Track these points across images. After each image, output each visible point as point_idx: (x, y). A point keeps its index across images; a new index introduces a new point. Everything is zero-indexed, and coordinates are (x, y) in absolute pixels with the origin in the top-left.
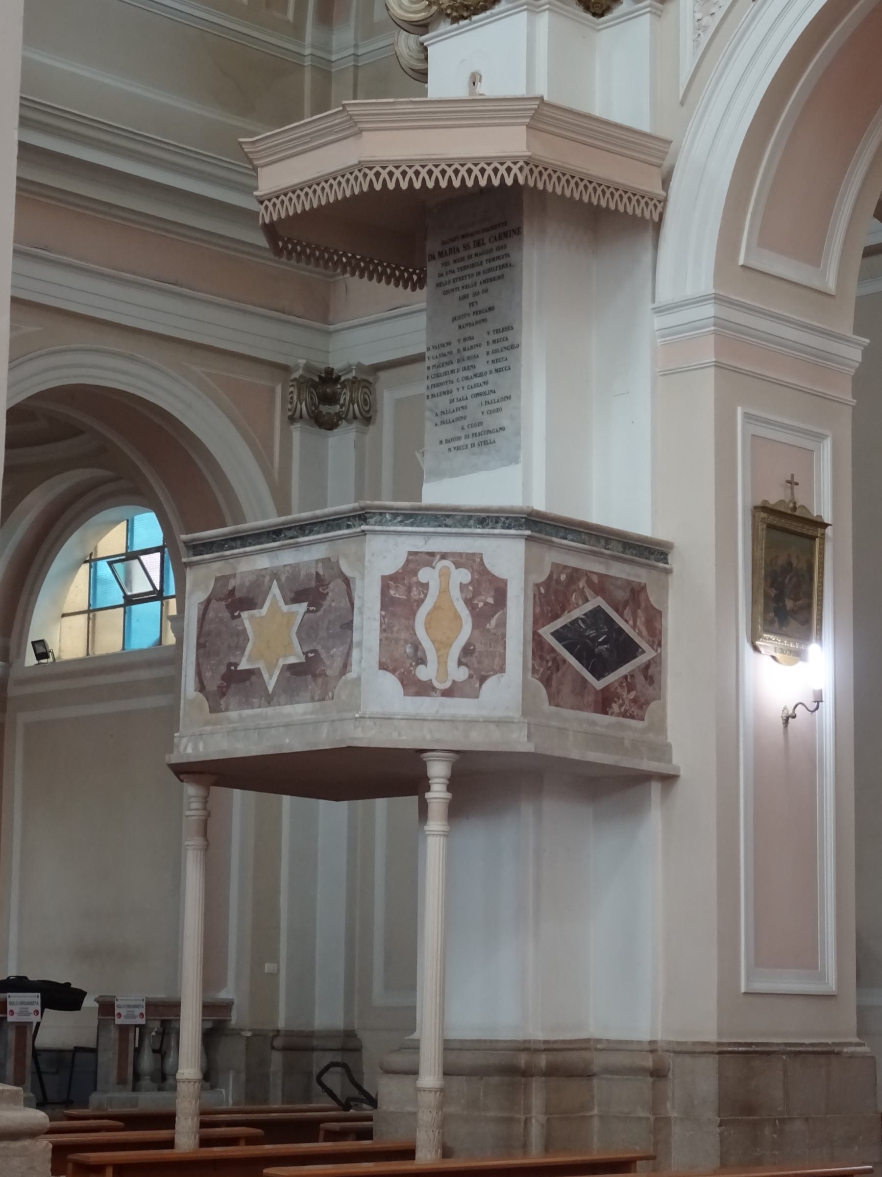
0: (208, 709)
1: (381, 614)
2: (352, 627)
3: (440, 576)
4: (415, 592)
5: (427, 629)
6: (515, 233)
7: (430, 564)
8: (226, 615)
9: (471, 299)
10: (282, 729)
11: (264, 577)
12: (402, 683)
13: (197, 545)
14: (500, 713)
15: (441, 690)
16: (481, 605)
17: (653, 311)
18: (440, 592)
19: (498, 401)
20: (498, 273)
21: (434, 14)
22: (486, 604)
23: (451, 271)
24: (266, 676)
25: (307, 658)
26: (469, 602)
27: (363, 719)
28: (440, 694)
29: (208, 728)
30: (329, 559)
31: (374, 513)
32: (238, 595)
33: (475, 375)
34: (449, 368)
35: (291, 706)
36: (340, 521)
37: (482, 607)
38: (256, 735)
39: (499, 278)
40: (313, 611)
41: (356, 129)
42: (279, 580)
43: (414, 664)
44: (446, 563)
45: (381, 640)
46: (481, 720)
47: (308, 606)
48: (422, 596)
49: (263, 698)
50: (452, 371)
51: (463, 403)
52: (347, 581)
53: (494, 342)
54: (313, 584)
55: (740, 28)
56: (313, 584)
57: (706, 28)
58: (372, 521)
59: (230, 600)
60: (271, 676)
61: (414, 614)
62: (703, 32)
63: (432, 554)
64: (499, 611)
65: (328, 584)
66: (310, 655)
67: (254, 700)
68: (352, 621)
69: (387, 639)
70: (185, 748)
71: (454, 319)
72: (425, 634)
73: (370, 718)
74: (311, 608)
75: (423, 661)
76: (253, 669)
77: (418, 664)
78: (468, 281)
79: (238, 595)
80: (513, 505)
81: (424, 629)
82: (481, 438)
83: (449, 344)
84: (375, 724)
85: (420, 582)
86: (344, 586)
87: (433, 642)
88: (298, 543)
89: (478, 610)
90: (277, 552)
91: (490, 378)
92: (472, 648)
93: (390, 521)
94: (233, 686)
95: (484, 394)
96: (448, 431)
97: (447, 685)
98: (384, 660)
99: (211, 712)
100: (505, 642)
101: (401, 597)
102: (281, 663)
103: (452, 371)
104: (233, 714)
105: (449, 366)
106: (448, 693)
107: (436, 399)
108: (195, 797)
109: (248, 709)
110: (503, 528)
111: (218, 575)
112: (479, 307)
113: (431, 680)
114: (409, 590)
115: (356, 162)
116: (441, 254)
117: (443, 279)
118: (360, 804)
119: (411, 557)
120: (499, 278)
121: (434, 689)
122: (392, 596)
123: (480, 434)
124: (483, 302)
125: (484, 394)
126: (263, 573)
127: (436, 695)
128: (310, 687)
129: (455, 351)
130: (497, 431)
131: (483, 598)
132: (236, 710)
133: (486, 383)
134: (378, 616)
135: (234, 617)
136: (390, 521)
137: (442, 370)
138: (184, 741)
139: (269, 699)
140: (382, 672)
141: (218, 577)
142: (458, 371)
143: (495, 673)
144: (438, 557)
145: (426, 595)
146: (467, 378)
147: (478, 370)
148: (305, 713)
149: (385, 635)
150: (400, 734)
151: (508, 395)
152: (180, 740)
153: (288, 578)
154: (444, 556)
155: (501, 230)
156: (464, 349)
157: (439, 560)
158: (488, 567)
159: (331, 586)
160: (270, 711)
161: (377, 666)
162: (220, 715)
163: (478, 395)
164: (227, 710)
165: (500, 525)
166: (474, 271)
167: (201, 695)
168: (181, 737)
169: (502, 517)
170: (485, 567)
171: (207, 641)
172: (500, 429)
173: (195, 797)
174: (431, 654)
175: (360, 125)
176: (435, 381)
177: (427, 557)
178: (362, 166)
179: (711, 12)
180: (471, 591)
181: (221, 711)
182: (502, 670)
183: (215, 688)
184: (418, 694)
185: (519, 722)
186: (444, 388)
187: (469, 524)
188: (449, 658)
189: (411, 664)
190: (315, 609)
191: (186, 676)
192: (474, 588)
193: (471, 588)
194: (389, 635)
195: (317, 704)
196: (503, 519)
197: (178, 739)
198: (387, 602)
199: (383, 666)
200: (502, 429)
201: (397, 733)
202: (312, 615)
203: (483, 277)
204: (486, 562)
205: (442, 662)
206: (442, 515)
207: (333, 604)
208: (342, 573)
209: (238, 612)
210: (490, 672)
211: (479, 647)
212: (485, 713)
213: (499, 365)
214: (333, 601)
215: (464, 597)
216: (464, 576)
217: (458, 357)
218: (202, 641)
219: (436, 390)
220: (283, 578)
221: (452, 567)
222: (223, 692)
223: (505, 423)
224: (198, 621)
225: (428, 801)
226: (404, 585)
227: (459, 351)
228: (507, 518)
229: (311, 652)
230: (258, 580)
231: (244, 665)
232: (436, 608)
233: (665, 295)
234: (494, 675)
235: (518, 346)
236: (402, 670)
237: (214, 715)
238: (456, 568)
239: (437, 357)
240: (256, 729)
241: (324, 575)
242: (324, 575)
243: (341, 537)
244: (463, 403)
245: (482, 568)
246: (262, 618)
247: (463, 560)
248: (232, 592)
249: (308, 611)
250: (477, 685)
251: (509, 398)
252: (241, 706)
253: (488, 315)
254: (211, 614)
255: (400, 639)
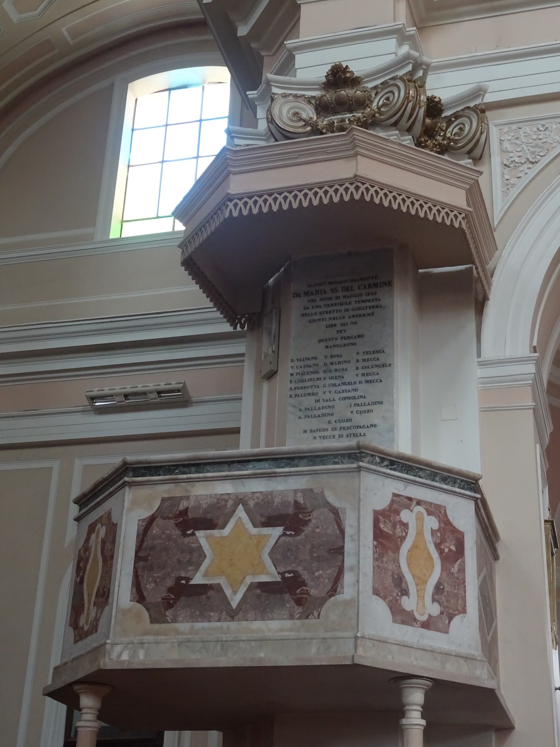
0: (149, 619)
1: (373, 544)
2: (344, 552)
3: (417, 519)
4: (398, 530)
5: (409, 565)
6: (386, 285)
7: (408, 507)
8: (176, 532)
9: (339, 328)
10: (253, 644)
11: (227, 501)
12: (391, 609)
13: (138, 468)
14: (464, 650)
15: (421, 622)
16: (446, 550)
17: (478, 364)
18: (417, 533)
19: (369, 404)
20: (368, 311)
21: (308, 131)
22: (450, 550)
23: (317, 307)
24: (228, 592)
25: (283, 578)
26: (438, 546)
27: (364, 639)
28: (420, 625)
29: (150, 638)
30: (312, 490)
31: (368, 454)
32: (190, 515)
33: (344, 384)
34: (315, 376)
35: (263, 622)
36: (325, 458)
37: (447, 552)
38: (219, 647)
39: (369, 315)
40: (290, 535)
41: (353, 152)
42: (245, 505)
43: (399, 594)
44: (420, 509)
45: (374, 568)
46: (454, 654)
47: (284, 530)
48: (404, 534)
49: (224, 613)
50: (318, 379)
51: (331, 404)
52: (335, 512)
53: (364, 360)
54: (291, 510)
55: (552, 186)
56: (291, 510)
57: (513, 185)
58: (366, 460)
59: (182, 519)
60: (235, 593)
61: (397, 549)
62: (511, 187)
63: (410, 499)
64: (460, 559)
65: (311, 512)
66: (287, 575)
67: (212, 614)
68: (343, 547)
69: (379, 567)
70: (120, 655)
71: (320, 341)
72: (407, 568)
73: (370, 639)
74: (288, 533)
75: (405, 592)
76: (211, 584)
77: (403, 595)
78: (335, 315)
79: (190, 515)
80: (469, 470)
81: (406, 565)
82: (350, 431)
83: (315, 358)
84: (373, 645)
85: (402, 521)
86: (332, 515)
87: (414, 576)
88: (276, 473)
89: (444, 554)
90: (244, 480)
91: (361, 387)
92: (442, 587)
93: (379, 463)
94: (183, 598)
95: (354, 398)
96: (307, 424)
97: (425, 618)
98: (376, 586)
99: (151, 622)
100: (465, 586)
101: (388, 531)
102: (249, 580)
103: (318, 379)
104: (184, 626)
105: (314, 375)
106: (426, 625)
107: (301, 399)
108: (90, 708)
109: (202, 622)
110: (459, 488)
111: (166, 496)
112: (348, 334)
113: (413, 611)
114: (394, 526)
115: (351, 175)
116: (306, 294)
117: (307, 311)
118: (200, 734)
119: (394, 498)
120: (369, 315)
121: (415, 620)
122: (381, 529)
123: (348, 428)
124: (352, 331)
125: (354, 398)
126: (226, 497)
127: (417, 625)
128: (288, 605)
129: (321, 364)
130: (368, 427)
131: (448, 544)
132: (187, 622)
133: (356, 390)
134: (371, 546)
135: (185, 535)
136: (379, 463)
137: (307, 377)
138: (118, 649)
139: (233, 615)
140: (375, 597)
141: (165, 498)
142: (325, 379)
143: (460, 613)
144: (415, 502)
145: (407, 534)
146: (334, 385)
147: (346, 380)
148: (281, 630)
149: (377, 563)
150: (393, 658)
151: (379, 400)
152: (112, 648)
153: (257, 504)
154: (419, 503)
155: (371, 281)
156: (332, 363)
157: (415, 506)
158: (450, 518)
159: (315, 514)
160: (233, 625)
161: (371, 591)
162: (163, 626)
163: (345, 398)
164: (174, 621)
165: (457, 485)
166: (343, 308)
167: (139, 606)
168: (114, 644)
169: (458, 479)
170: (448, 519)
171: (149, 555)
172: (372, 425)
173: (90, 708)
174: (412, 588)
175: (358, 149)
176: (300, 385)
177: (407, 500)
178: (356, 179)
179: (518, 176)
180: (439, 537)
181: (167, 622)
182: (464, 611)
183: (159, 600)
184: (403, 622)
185: (481, 661)
186: (310, 391)
187: (436, 480)
188: (426, 593)
189: (398, 594)
190: (293, 533)
191: (119, 586)
192: (441, 534)
193: (439, 534)
194: (380, 564)
195: (298, 622)
196: (459, 481)
197: (110, 646)
198: (378, 534)
199: (376, 592)
200: (375, 426)
201: (391, 657)
202: (289, 539)
203: (351, 313)
204: (449, 514)
205: (421, 597)
206: (417, 468)
207: (317, 530)
208: (328, 503)
209: (192, 530)
210: (455, 611)
211: (447, 588)
212: (453, 648)
213: (369, 378)
214: (317, 527)
215: (434, 542)
216: (432, 523)
217: (325, 368)
218: (142, 554)
219: (299, 392)
220: (251, 503)
221: (425, 513)
222: (168, 604)
223: (376, 421)
224: (138, 536)
225: (404, 727)
226: (390, 521)
227: (325, 364)
228: (462, 481)
229: (289, 572)
230: (218, 503)
231: (198, 579)
232: (415, 546)
233: (488, 352)
234: (459, 614)
235: (390, 365)
236: (391, 598)
237: (156, 626)
238: (428, 515)
239: (301, 367)
240: (218, 641)
241: (305, 503)
242: (305, 503)
243: (328, 472)
244: (331, 404)
245: (446, 519)
246: (223, 538)
247: (432, 509)
248: (185, 512)
249: (284, 534)
250: (447, 622)
251: (381, 403)
252: (193, 618)
253: (358, 341)
254: (155, 530)
255: (389, 570)
